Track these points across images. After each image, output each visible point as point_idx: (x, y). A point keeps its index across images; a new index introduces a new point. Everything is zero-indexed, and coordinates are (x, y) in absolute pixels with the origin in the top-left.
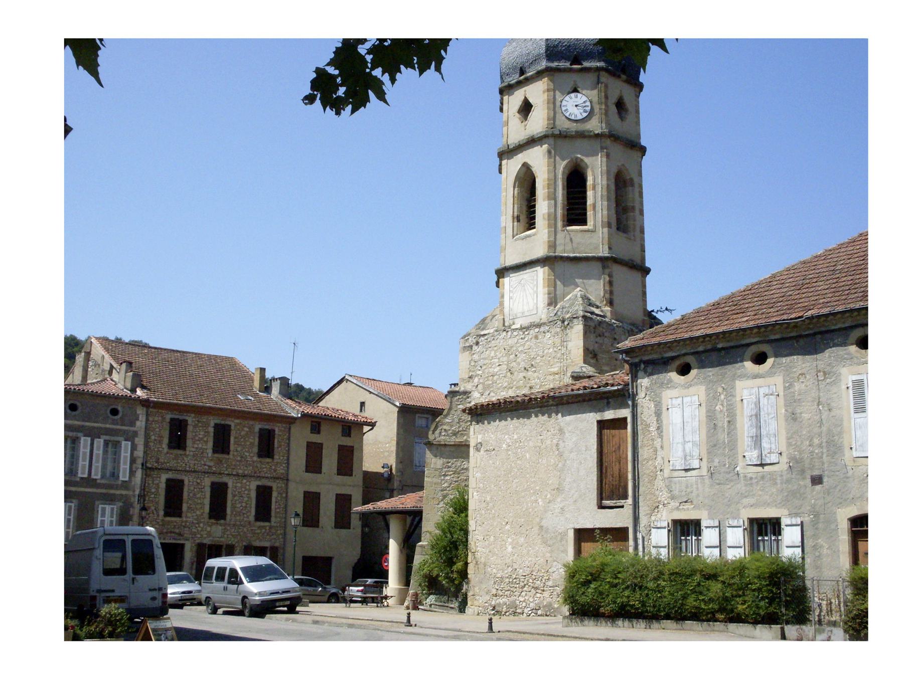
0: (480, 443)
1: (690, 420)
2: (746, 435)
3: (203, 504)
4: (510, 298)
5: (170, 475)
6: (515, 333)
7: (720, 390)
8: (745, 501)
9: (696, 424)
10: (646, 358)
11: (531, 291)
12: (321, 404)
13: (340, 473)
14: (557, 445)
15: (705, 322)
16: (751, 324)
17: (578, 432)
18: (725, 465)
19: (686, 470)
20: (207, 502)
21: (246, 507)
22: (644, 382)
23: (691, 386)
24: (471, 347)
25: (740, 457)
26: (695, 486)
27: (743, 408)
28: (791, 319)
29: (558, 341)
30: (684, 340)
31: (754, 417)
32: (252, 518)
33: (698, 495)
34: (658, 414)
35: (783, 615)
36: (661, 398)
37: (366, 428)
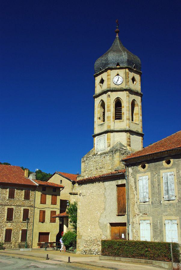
0: (81, 193)
1: (145, 184)
2: (164, 189)
3: (4, 215)
4: (97, 145)
5: (24, 208)
6: (98, 156)
7: (155, 174)
8: (164, 214)
9: (147, 186)
10: (131, 163)
11: (103, 142)
12: (48, 181)
13: (41, 203)
14: (104, 193)
15: (151, 150)
16: (165, 150)
17: (110, 189)
18: (157, 200)
19: (144, 202)
20: (6, 215)
21: (19, 216)
22: (130, 170)
23: (145, 172)
24: (85, 161)
25: (162, 197)
26: (147, 208)
27: (163, 180)
28: (178, 148)
29: (111, 158)
30: (143, 156)
31: (166, 183)
32: (21, 220)
33: (148, 211)
34: (135, 183)
35: (74, 244)
36: (136, 177)
37: (61, 189)
